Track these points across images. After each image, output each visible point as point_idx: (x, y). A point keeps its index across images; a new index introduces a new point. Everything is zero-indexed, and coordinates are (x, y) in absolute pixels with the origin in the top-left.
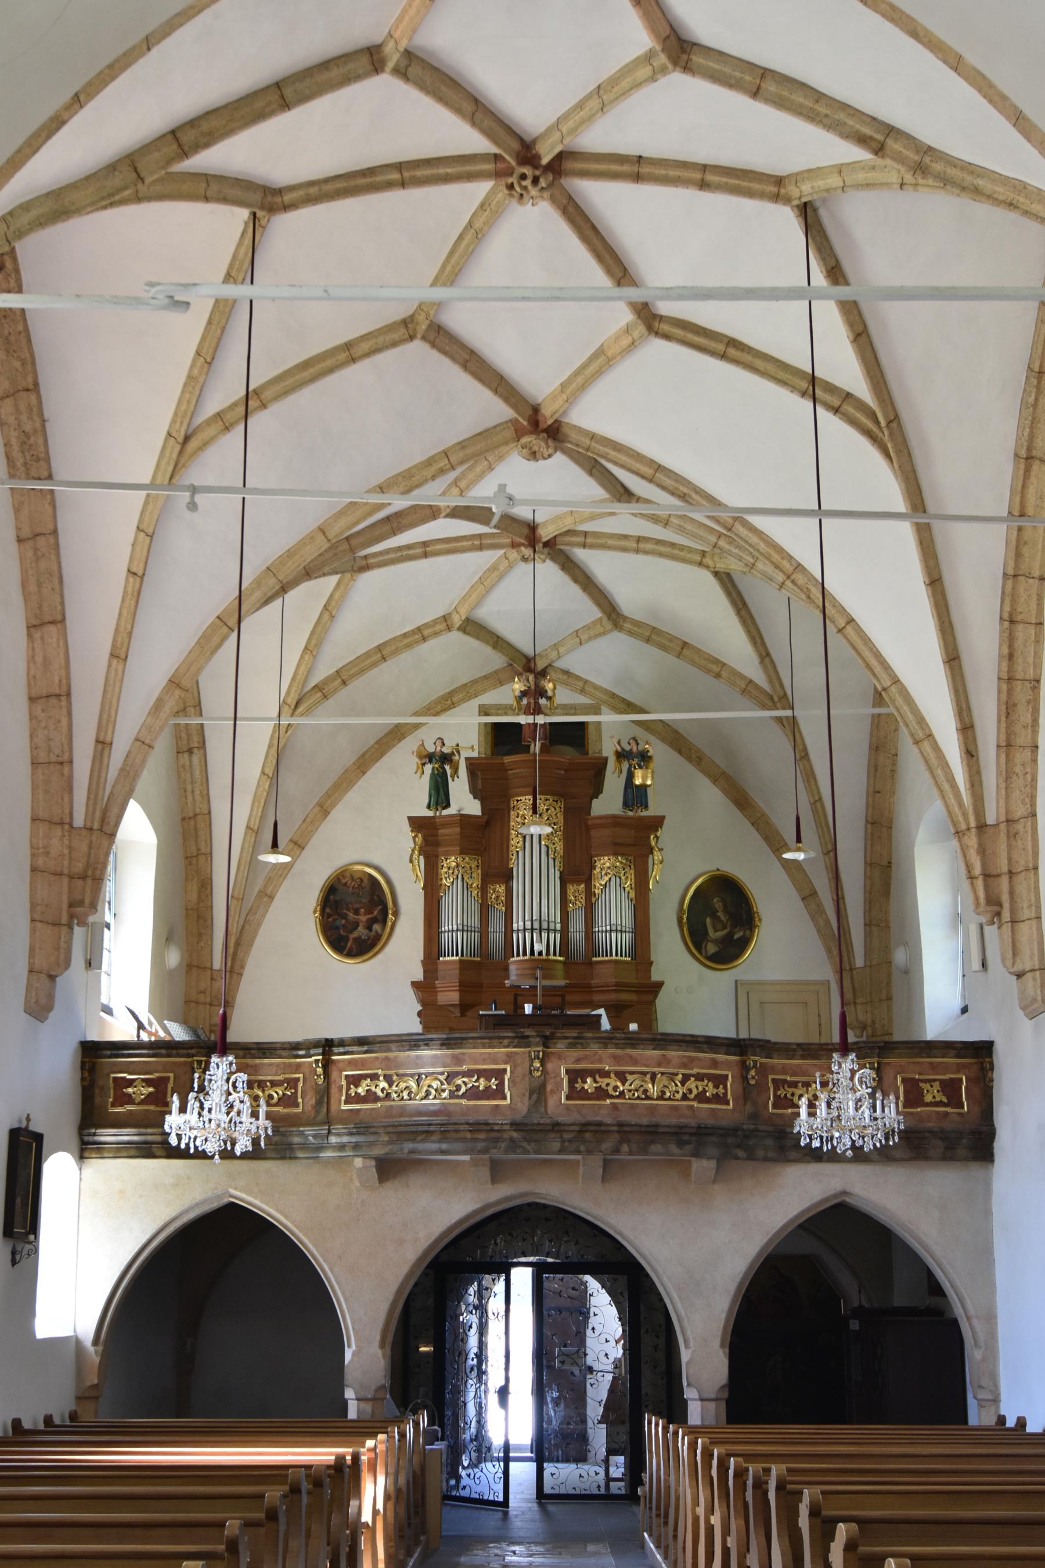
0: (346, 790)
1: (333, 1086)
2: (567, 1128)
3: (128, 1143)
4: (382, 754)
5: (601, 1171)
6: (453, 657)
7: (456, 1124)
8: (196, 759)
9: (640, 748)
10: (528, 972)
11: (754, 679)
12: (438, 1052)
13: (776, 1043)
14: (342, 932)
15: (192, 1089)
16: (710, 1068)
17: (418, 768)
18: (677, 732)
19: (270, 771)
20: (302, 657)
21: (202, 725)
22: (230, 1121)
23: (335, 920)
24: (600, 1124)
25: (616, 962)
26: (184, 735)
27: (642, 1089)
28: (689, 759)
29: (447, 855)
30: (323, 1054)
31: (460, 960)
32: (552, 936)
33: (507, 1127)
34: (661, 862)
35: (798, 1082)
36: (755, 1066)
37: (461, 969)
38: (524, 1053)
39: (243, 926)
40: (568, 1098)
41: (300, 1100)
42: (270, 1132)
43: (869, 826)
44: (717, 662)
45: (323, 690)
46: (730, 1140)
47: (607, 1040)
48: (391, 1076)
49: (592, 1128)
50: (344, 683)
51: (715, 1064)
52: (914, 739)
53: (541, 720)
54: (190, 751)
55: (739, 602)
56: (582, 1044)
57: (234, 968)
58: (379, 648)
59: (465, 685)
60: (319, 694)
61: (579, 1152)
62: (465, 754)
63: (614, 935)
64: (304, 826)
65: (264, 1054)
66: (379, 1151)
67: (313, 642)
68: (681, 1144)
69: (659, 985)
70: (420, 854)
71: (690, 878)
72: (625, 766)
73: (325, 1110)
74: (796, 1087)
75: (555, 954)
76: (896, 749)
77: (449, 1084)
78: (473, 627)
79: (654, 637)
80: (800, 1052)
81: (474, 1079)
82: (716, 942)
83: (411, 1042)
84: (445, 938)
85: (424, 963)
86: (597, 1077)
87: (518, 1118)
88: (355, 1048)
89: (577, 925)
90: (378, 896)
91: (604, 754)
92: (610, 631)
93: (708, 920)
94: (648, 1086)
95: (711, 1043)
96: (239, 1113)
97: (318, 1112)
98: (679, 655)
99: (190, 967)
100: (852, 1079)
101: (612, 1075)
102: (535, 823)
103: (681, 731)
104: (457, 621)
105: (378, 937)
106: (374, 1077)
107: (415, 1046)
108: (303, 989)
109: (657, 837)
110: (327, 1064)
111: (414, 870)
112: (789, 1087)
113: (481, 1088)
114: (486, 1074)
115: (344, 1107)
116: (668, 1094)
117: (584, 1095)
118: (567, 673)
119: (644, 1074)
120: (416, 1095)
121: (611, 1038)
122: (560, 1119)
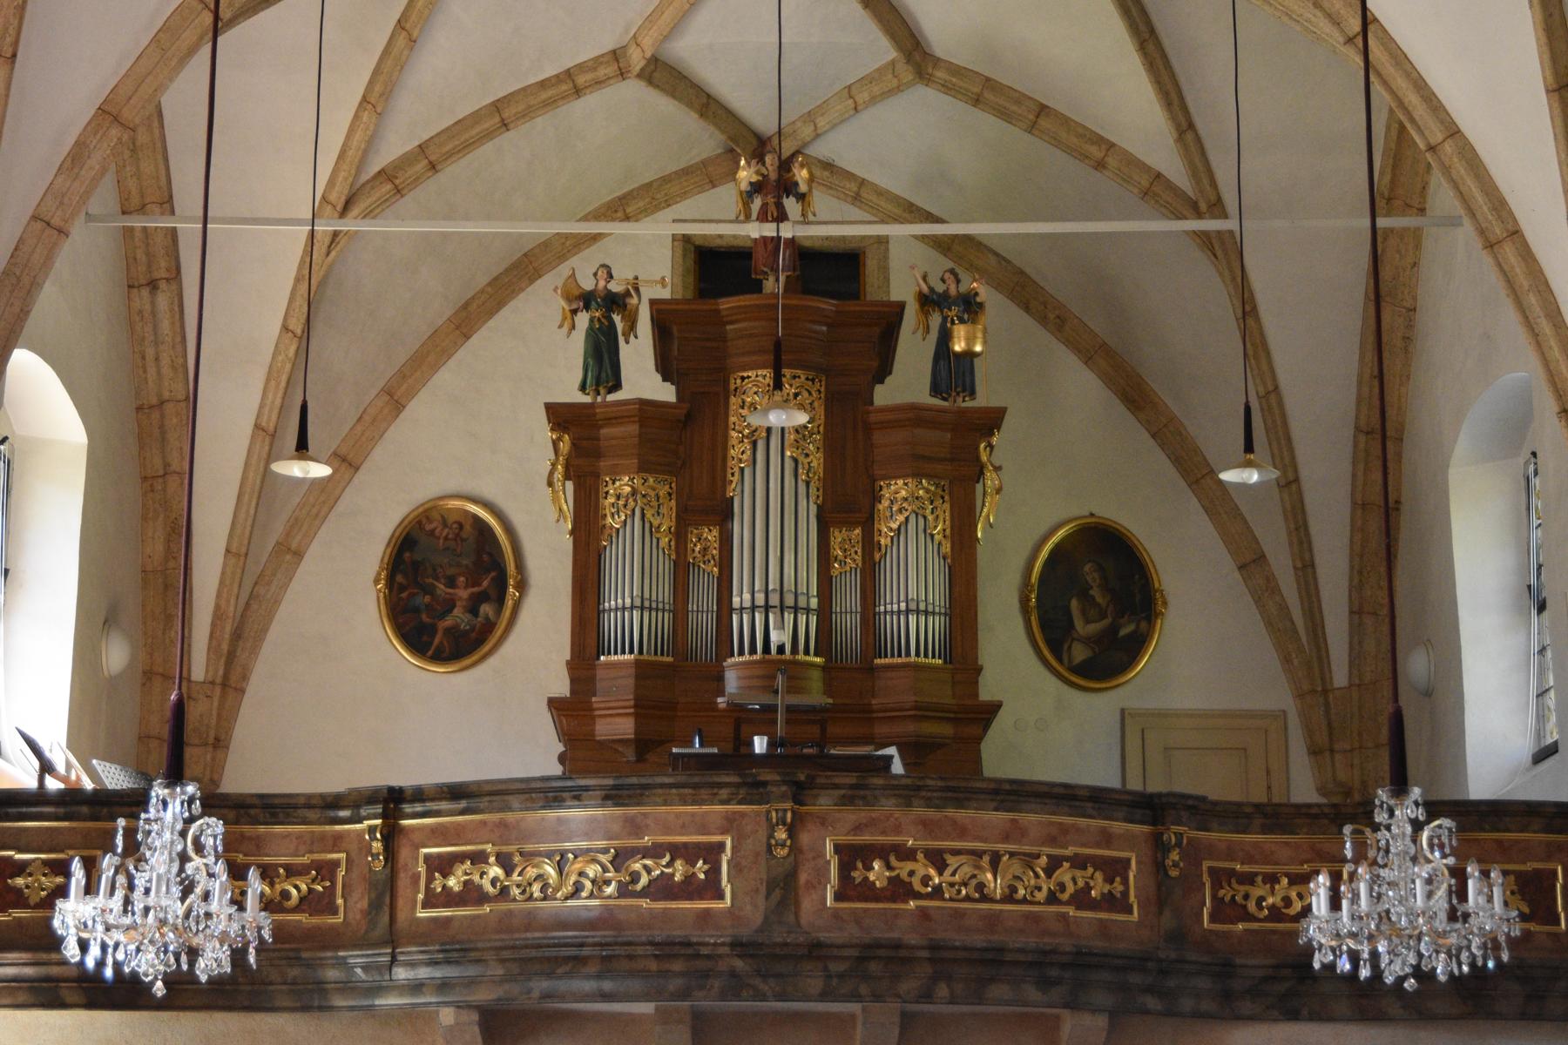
0: (435, 368)
1: (402, 875)
2: (835, 952)
3: (15, 979)
4: (500, 305)
5: (897, 1031)
6: (627, 128)
7: (630, 944)
8: (163, 300)
9: (963, 289)
10: (756, 682)
11: (1165, 173)
12: (599, 812)
13: (1215, 803)
14: (424, 617)
15: (111, 848)
16: (1098, 845)
17: (565, 318)
18: (1022, 272)
19: (297, 326)
20: (356, 117)
21: (175, 229)
22: (187, 916)
23: (412, 595)
24: (897, 946)
25: (917, 667)
26: (140, 255)
27: (974, 882)
28: (1043, 320)
29: (615, 473)
30: (384, 816)
31: (637, 663)
32: (802, 619)
33: (726, 950)
34: (999, 491)
35: (1256, 874)
36: (1179, 844)
37: (637, 677)
38: (758, 814)
39: (248, 604)
40: (839, 897)
41: (340, 901)
42: (266, 934)
43: (1362, 438)
44: (1099, 140)
45: (394, 182)
46: (1135, 979)
47: (907, 793)
48: (510, 856)
49: (882, 952)
50: (433, 167)
51: (1107, 839)
52: (1487, 240)
53: (787, 231)
54: (153, 285)
55: (1142, 27)
56: (863, 797)
57: (231, 680)
58: (497, 106)
59: (650, 184)
60: (389, 186)
61: (855, 997)
62: (649, 293)
63: (912, 619)
64: (359, 428)
65: (274, 815)
66: (484, 995)
67: (378, 88)
68: (1045, 983)
69: (994, 708)
70: (567, 477)
71: (1043, 529)
72: (936, 320)
73: (386, 919)
74: (1252, 883)
75: (807, 652)
76: (1415, 298)
77: (617, 870)
78: (663, 74)
79: (988, 95)
80: (1258, 822)
81: (664, 862)
82: (1087, 641)
83: (546, 793)
84: (611, 622)
85: (572, 666)
86: (893, 859)
87: (745, 933)
88: (444, 805)
89: (848, 601)
90: (490, 555)
91: (895, 296)
92: (909, 85)
93: (1074, 604)
94: (980, 876)
95: (1096, 800)
96: (206, 896)
97: (372, 923)
98: (1032, 128)
99: (148, 675)
100: (1415, 839)
101: (920, 856)
102: (777, 406)
103: (1028, 270)
104: (637, 60)
105: (489, 627)
106: (478, 858)
107: (555, 799)
108: (346, 703)
109: (991, 446)
110: (391, 835)
111: (555, 500)
112: (1240, 883)
113: (677, 878)
114: (687, 853)
115: (422, 914)
116: (1022, 892)
117: (867, 892)
118: (828, 166)
119: (978, 854)
120: (557, 890)
121: (919, 788)
122: (823, 936)
